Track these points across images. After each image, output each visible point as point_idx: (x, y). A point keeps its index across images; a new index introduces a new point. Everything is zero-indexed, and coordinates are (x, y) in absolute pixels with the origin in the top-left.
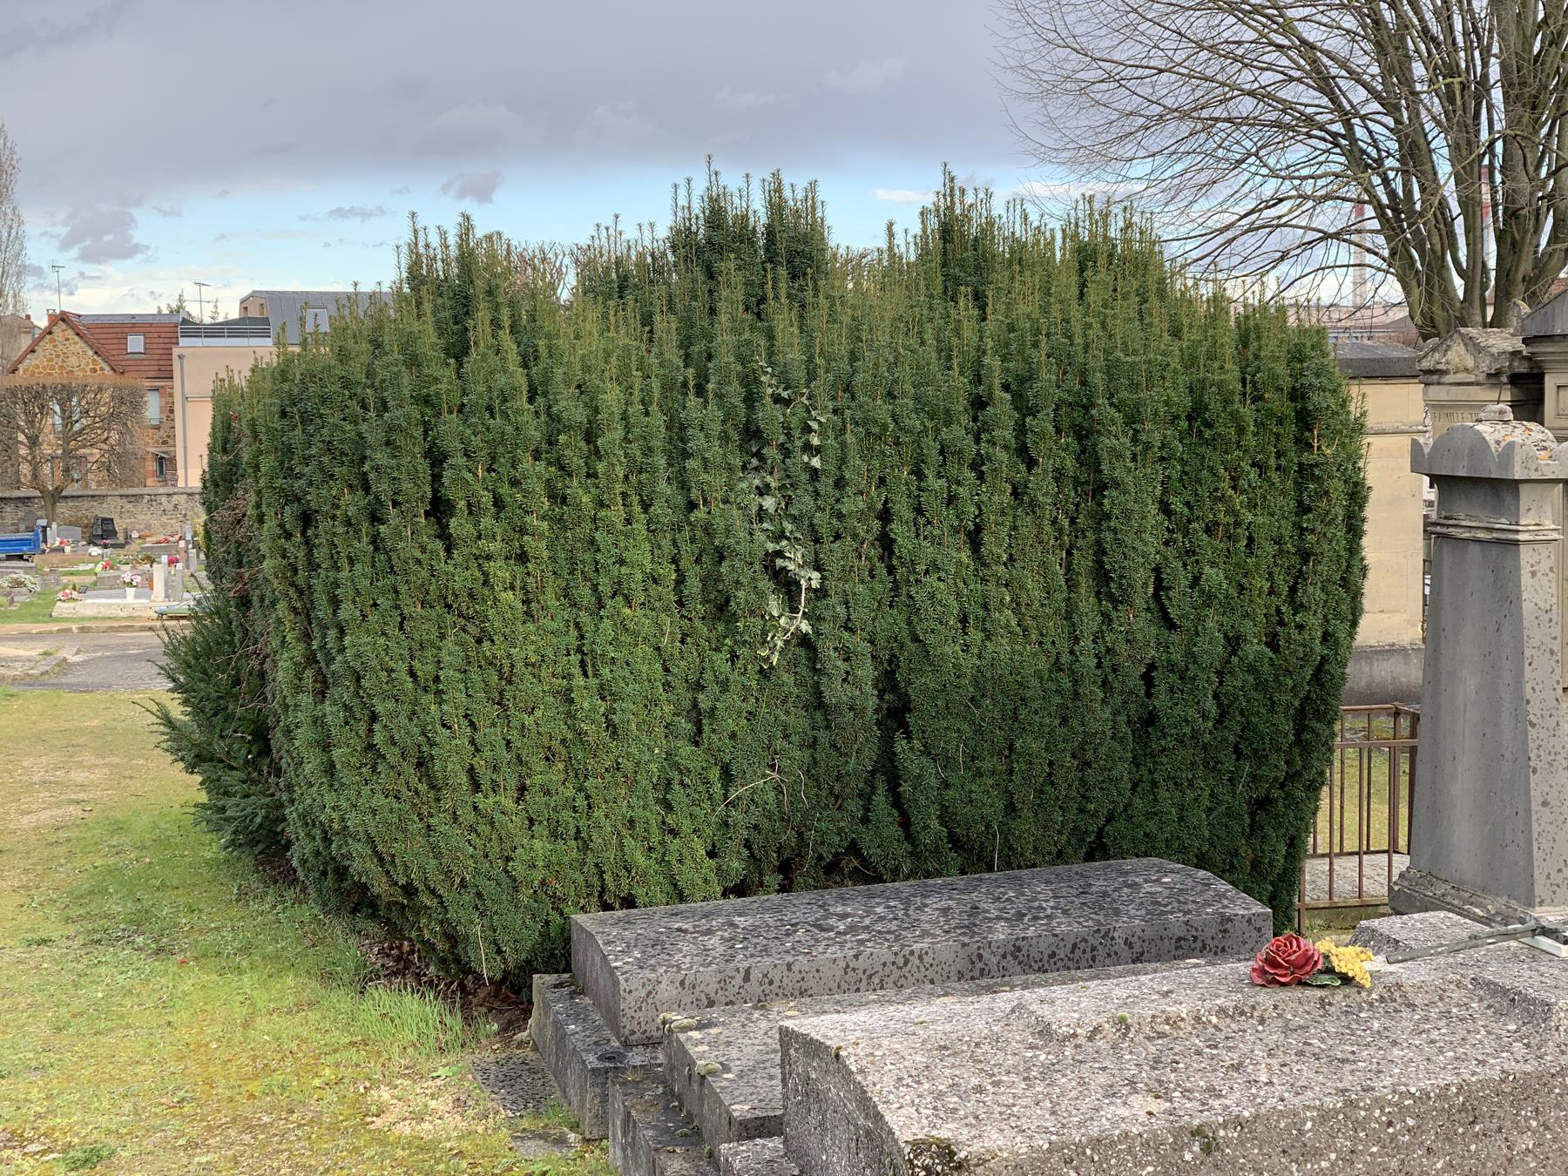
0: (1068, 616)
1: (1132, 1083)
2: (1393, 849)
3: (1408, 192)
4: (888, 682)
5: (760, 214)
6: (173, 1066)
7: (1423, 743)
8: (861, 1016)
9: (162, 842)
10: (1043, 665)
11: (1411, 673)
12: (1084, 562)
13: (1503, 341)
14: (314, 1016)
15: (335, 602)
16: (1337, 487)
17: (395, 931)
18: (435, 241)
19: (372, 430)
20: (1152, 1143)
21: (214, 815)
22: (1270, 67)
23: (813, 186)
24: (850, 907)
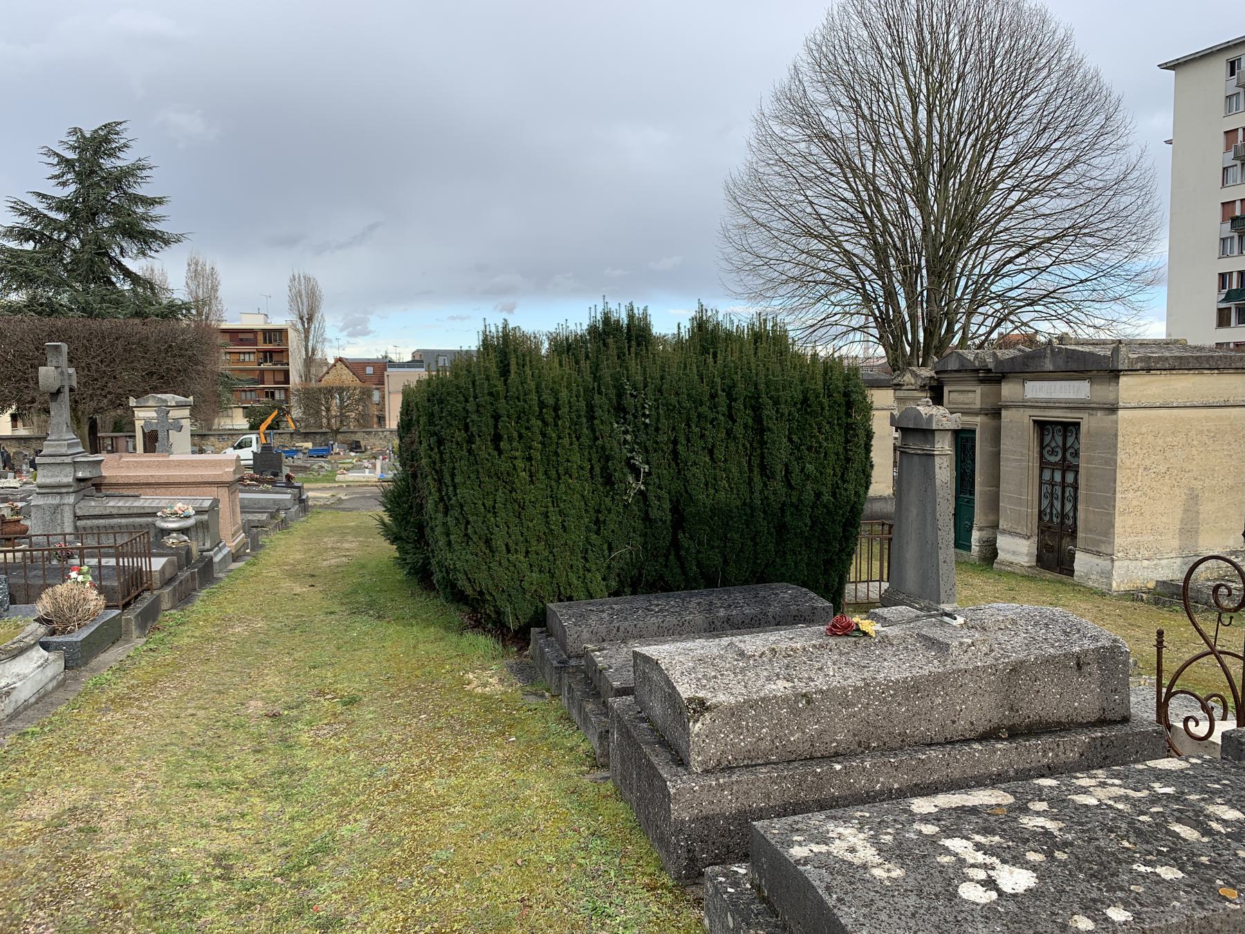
0: (749, 484)
1: (778, 675)
2: (881, 580)
3: (887, 310)
4: (675, 509)
5: (624, 320)
6: (385, 664)
7: (894, 535)
8: (666, 647)
9: (381, 573)
10: (739, 503)
11: (890, 508)
12: (756, 462)
13: (927, 373)
14: (442, 644)
15: (453, 476)
16: (862, 433)
17: (475, 610)
18: (493, 330)
19: (471, 407)
20: (786, 699)
21: (401, 562)
22: (832, 260)
23: (645, 309)
24: (659, 602)
